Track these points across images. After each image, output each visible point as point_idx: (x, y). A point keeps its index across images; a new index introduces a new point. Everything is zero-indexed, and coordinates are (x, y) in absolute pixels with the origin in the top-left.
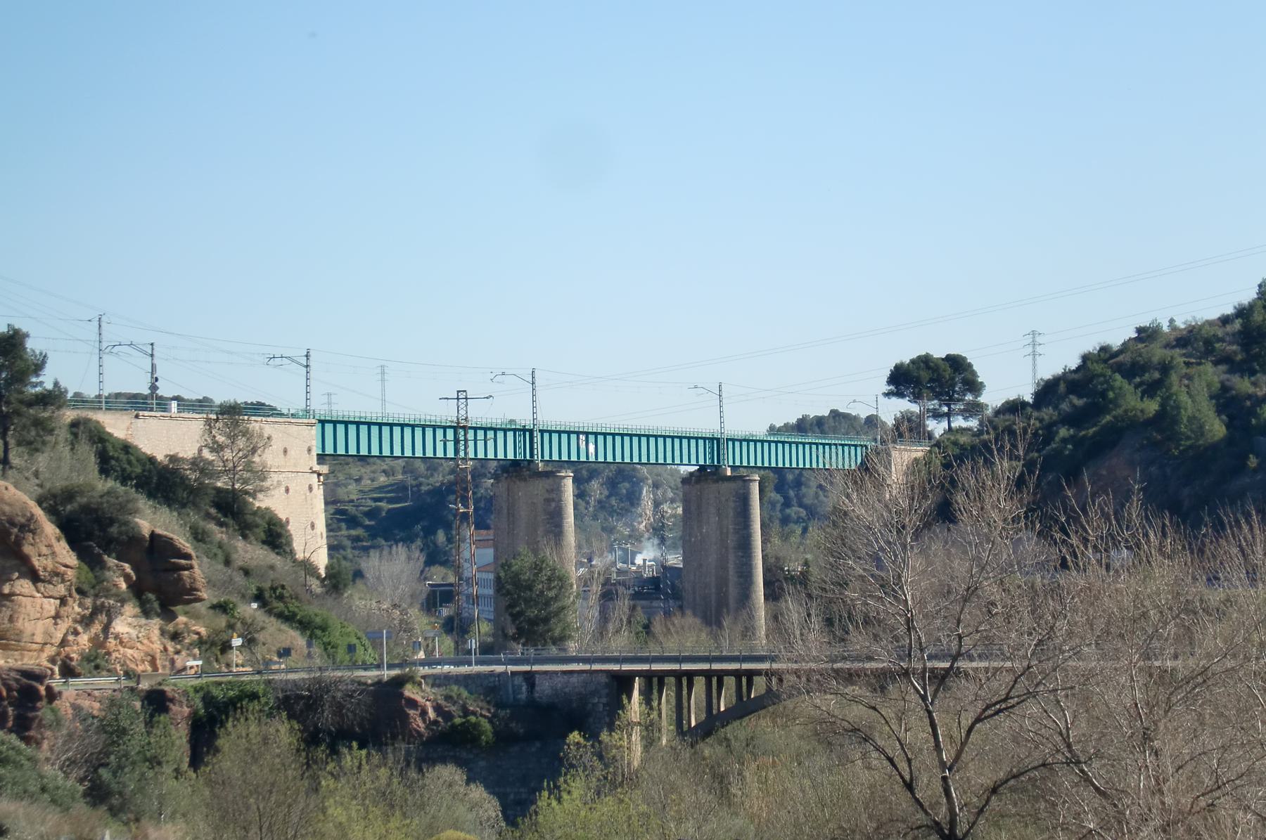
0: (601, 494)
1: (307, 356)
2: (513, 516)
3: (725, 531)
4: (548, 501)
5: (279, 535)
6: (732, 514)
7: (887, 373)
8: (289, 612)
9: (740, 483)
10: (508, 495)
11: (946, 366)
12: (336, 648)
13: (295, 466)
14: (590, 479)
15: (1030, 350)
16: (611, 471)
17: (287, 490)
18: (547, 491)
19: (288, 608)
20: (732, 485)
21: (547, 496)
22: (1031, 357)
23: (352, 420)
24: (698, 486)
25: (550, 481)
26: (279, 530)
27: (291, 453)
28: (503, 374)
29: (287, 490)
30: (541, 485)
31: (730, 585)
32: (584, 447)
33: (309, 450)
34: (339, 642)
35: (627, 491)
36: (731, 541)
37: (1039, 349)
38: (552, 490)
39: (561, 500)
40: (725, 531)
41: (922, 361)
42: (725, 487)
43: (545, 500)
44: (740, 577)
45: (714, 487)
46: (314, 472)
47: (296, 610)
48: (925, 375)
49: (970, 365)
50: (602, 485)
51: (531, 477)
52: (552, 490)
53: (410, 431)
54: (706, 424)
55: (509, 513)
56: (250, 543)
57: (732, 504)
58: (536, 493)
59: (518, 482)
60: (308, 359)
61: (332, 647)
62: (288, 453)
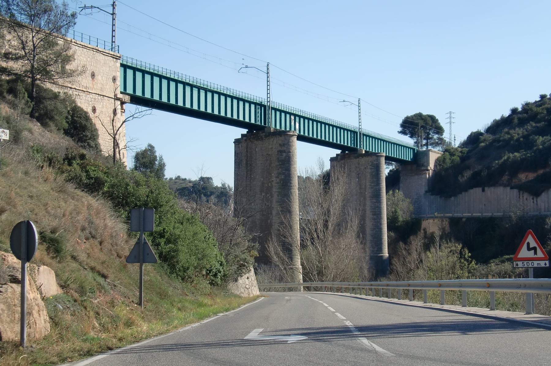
0: (215, 201)
1: (113, 5)
2: (251, 165)
3: (363, 187)
4: (280, 152)
5: (84, 128)
6: (369, 176)
7: (401, 121)
8: (89, 177)
9: (374, 158)
10: (247, 151)
11: (429, 119)
12: (175, 242)
13: (102, 90)
14: (211, 195)
15: (448, 120)
16: (219, 193)
17: (93, 75)
18: (280, 145)
19: (87, 172)
20: (369, 159)
21: (280, 149)
22: (449, 124)
23: (148, 70)
24: (343, 161)
25: (282, 138)
26: (84, 122)
27: (98, 77)
28: (247, 67)
29: (93, 75)
30: (275, 141)
31: (367, 219)
32: (293, 124)
33: (114, 79)
34: (177, 232)
35: (225, 200)
36: (368, 193)
37: (453, 120)
38: (284, 145)
39: (290, 152)
40: (363, 187)
41: (419, 116)
42: (363, 160)
43: (278, 151)
44: (373, 215)
45: (355, 161)
46: (117, 99)
47: (101, 175)
48: (421, 123)
49: (437, 120)
50: (215, 198)
51: (266, 136)
52: (284, 145)
53: (190, 89)
54: (351, 123)
55: (247, 164)
56: (51, 131)
57: (369, 171)
58: (270, 147)
59: (255, 142)
60: (114, 8)
61: (168, 242)
62: (96, 77)
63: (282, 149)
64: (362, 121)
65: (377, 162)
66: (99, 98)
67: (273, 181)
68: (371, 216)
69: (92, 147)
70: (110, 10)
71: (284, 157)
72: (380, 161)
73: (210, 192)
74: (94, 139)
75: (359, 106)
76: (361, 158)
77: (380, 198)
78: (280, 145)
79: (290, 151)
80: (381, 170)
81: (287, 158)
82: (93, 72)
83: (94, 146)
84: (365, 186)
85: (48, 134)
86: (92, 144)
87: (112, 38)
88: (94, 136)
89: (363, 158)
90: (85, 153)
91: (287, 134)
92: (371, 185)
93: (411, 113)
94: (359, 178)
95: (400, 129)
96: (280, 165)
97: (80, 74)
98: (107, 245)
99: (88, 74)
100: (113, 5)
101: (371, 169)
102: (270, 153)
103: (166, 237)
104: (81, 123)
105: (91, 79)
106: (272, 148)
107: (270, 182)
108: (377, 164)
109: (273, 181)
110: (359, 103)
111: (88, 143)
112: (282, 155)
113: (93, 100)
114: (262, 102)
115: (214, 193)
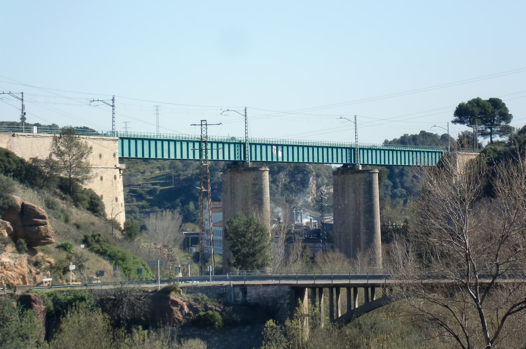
0: (285, 180)
1: (113, 100)
3: (358, 202)
4: (254, 185)
5: (97, 205)
14: (279, 172)
16: (291, 167)
18: (254, 179)
24: (342, 176)
25: (256, 173)
26: (97, 202)
27: (104, 156)
28: (228, 110)
29: (102, 179)
32: (276, 153)
34: (132, 267)
38: (257, 179)
39: (262, 184)
40: (358, 202)
41: (476, 103)
42: (358, 176)
44: (367, 229)
46: (117, 168)
48: (477, 110)
49: (504, 104)
50: (286, 175)
51: (244, 170)
52: (257, 179)
55: (231, 192)
56: (80, 210)
57: (362, 187)
58: (247, 180)
61: (128, 271)
62: (102, 157)
63: (256, 182)
64: (359, 137)
65: (370, 179)
66: (105, 170)
67: (249, 208)
68: (365, 231)
69: (102, 215)
70: (111, 103)
71: (257, 189)
72: (373, 177)
73: (278, 167)
74: (103, 211)
75: (355, 123)
76: (356, 174)
77: (373, 213)
78: (254, 179)
79: (262, 184)
80: (373, 186)
81: (260, 189)
82: (100, 154)
83: (103, 215)
84: (360, 201)
85: (79, 212)
86: (102, 213)
87: (113, 127)
88: (103, 209)
89: (357, 174)
90: (100, 233)
91: (260, 170)
92: (364, 201)
93: (466, 100)
94: (355, 193)
95: (454, 118)
96: (254, 195)
97: (94, 178)
98: (108, 273)
99: (99, 178)
100: (113, 100)
101: (364, 185)
102: (247, 185)
103: (116, 272)
104: (95, 203)
105: (99, 158)
106: (248, 181)
107: (247, 209)
108: (369, 180)
109: (249, 208)
110: (355, 120)
111: (100, 213)
112: (255, 187)
113: (101, 172)
114: (241, 141)
115: (284, 169)
